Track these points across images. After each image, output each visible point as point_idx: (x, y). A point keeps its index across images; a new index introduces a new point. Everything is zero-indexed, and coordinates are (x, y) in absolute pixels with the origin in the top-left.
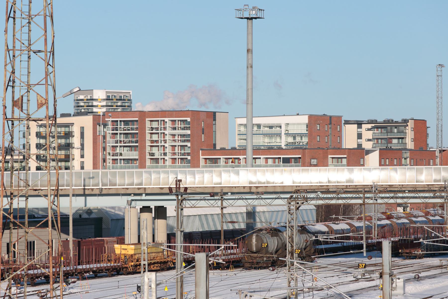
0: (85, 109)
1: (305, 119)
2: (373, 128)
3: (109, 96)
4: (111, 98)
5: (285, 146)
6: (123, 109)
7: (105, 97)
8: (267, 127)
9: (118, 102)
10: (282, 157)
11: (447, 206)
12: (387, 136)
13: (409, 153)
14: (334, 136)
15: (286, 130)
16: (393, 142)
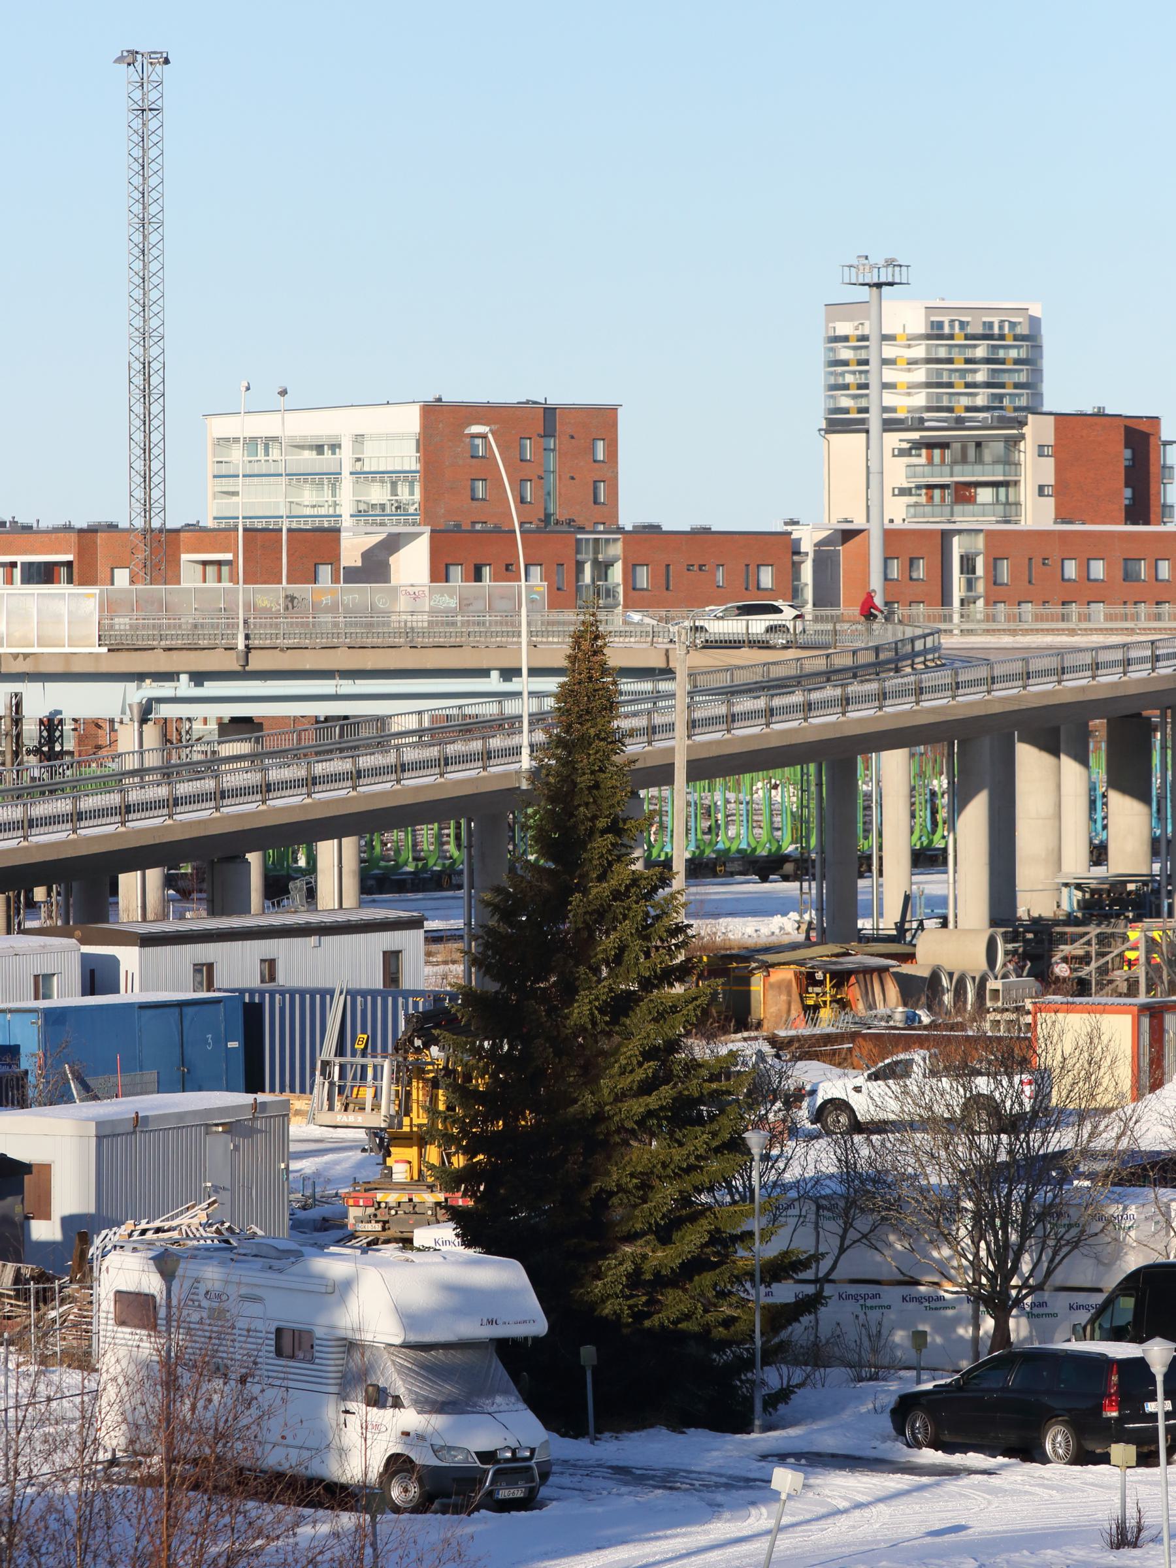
0: (854, 373)
1: (410, 421)
2: (917, 445)
3: (940, 325)
4: (947, 330)
5: (352, 516)
6: (994, 370)
7: (922, 329)
8: (310, 448)
9: (975, 346)
10: (20, 559)
11: (1169, 744)
12: (952, 476)
13: (620, 545)
14: (573, 478)
15: (358, 460)
16: (979, 499)
